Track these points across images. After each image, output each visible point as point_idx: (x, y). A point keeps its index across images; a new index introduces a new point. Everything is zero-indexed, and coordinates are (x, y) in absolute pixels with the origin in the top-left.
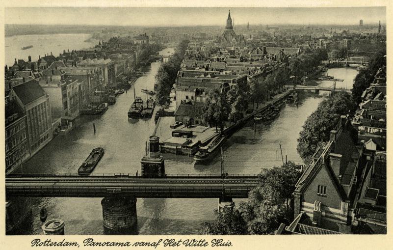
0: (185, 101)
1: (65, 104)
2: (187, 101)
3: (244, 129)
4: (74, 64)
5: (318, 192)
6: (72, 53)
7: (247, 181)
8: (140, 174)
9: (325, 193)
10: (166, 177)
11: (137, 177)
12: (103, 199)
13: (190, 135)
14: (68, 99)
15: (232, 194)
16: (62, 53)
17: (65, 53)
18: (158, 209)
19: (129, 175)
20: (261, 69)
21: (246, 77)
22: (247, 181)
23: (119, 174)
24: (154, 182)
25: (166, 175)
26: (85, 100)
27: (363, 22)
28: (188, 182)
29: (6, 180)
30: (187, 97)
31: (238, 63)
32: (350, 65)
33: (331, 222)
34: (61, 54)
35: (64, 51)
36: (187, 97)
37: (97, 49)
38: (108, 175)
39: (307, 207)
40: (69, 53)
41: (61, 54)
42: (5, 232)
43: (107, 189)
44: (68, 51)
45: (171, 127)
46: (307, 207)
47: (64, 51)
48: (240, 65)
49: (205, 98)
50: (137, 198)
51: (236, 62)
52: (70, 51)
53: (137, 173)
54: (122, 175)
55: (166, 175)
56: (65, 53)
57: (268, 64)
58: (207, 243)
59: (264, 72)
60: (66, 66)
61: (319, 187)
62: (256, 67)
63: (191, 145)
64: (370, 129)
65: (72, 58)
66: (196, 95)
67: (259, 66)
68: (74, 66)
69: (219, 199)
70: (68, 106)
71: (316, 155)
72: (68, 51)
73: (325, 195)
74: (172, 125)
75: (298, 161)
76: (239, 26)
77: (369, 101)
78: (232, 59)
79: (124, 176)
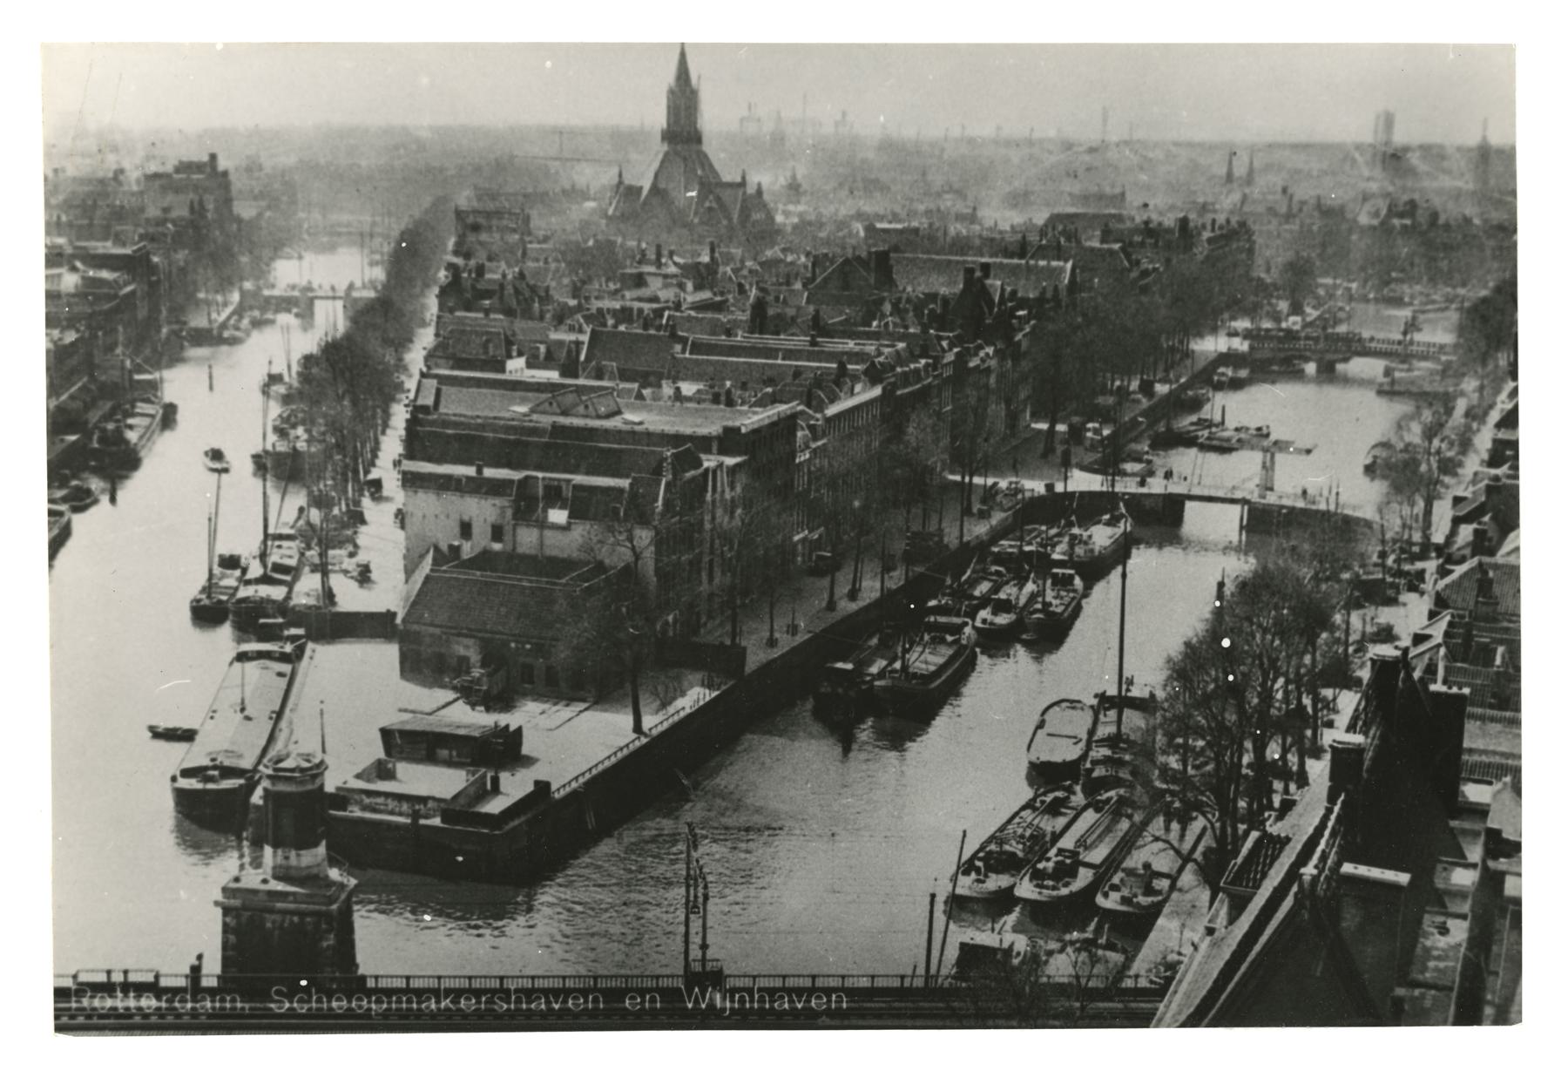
0: (455, 550)
2: (468, 550)
3: (739, 749)
19: (164, 982)
21: (793, 417)
23: (102, 978)
25: (363, 978)
30: (466, 529)
31: (740, 337)
36: (466, 529)
42: (49, 1021)
49: (1109, 531)
51: (729, 333)
54: (117, 978)
62: (842, 366)
63: (494, 806)
64: (1471, 751)
66: (515, 516)
75: (789, 229)
77: (1474, 562)
78: (709, 315)
79: (126, 987)
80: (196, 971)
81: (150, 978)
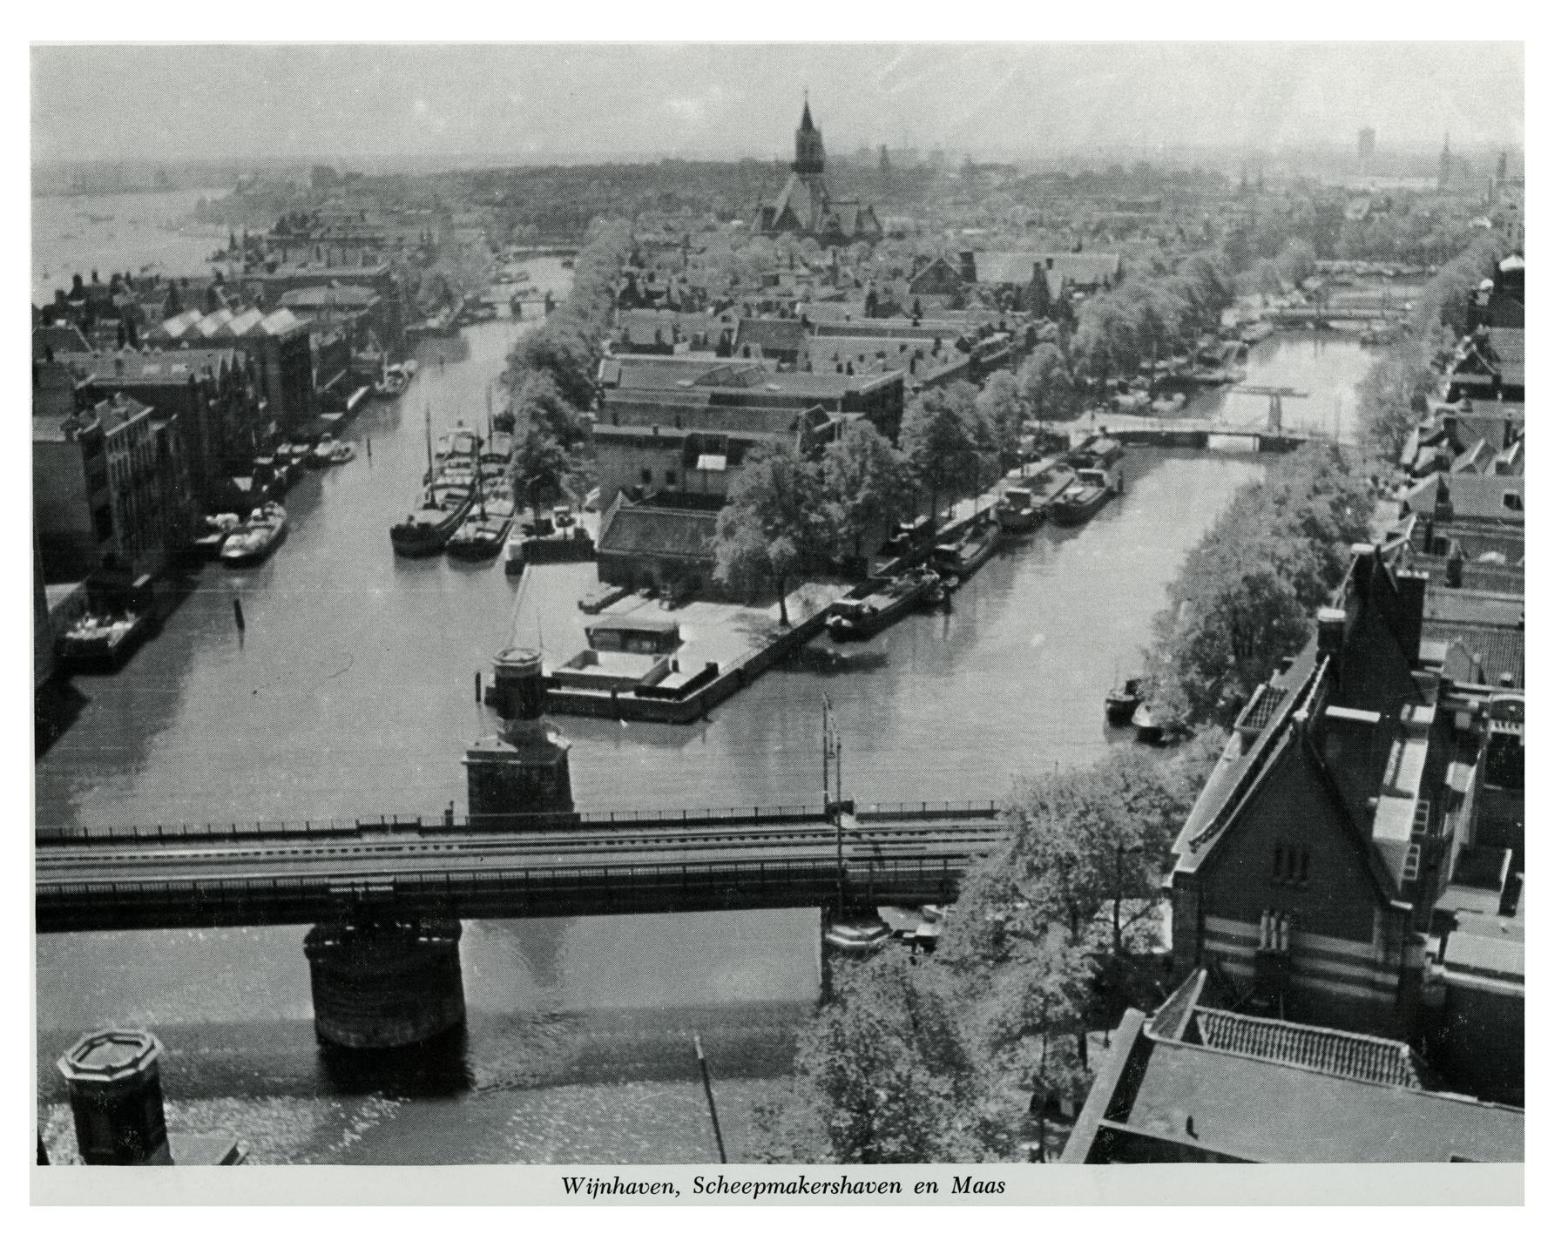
1: (102, 516)
4: (127, 335)
5: (1277, 872)
6: (115, 288)
7: (939, 831)
8: (461, 816)
9: (1304, 878)
10: (574, 824)
11: (449, 828)
12: (313, 931)
13: (667, 641)
14: (115, 495)
15: (879, 888)
16: (68, 287)
17: (79, 289)
18: (541, 962)
20: (963, 346)
22: (939, 831)
24: (523, 849)
25: (578, 816)
26: (185, 471)
27: (1378, 138)
28: (759, 841)
29: (1519, 719)
32: (1333, 324)
33: (1328, 994)
34: (60, 294)
35: (77, 279)
36: (646, 476)
37: (224, 268)
38: (633, 818)
39: (1226, 938)
40: (102, 289)
41: (60, 294)
43: (329, 886)
44: (95, 276)
45: (581, 606)
46: (1226, 938)
47: (77, 279)
48: (867, 332)
50: (466, 924)
52: (105, 278)
53: (449, 813)
54: (389, 821)
55: (578, 816)
56: (79, 289)
57: (990, 326)
58: (968, 1179)
59: (974, 362)
60: (94, 346)
61: (1278, 852)
65: (112, 311)
67: (951, 333)
68: (127, 346)
69: (818, 911)
70: (116, 523)
71: (1251, 714)
72: (95, 276)
73: (1304, 884)
74: (587, 603)
76: (843, 163)
80: (449, 813)
81: (414, 821)
